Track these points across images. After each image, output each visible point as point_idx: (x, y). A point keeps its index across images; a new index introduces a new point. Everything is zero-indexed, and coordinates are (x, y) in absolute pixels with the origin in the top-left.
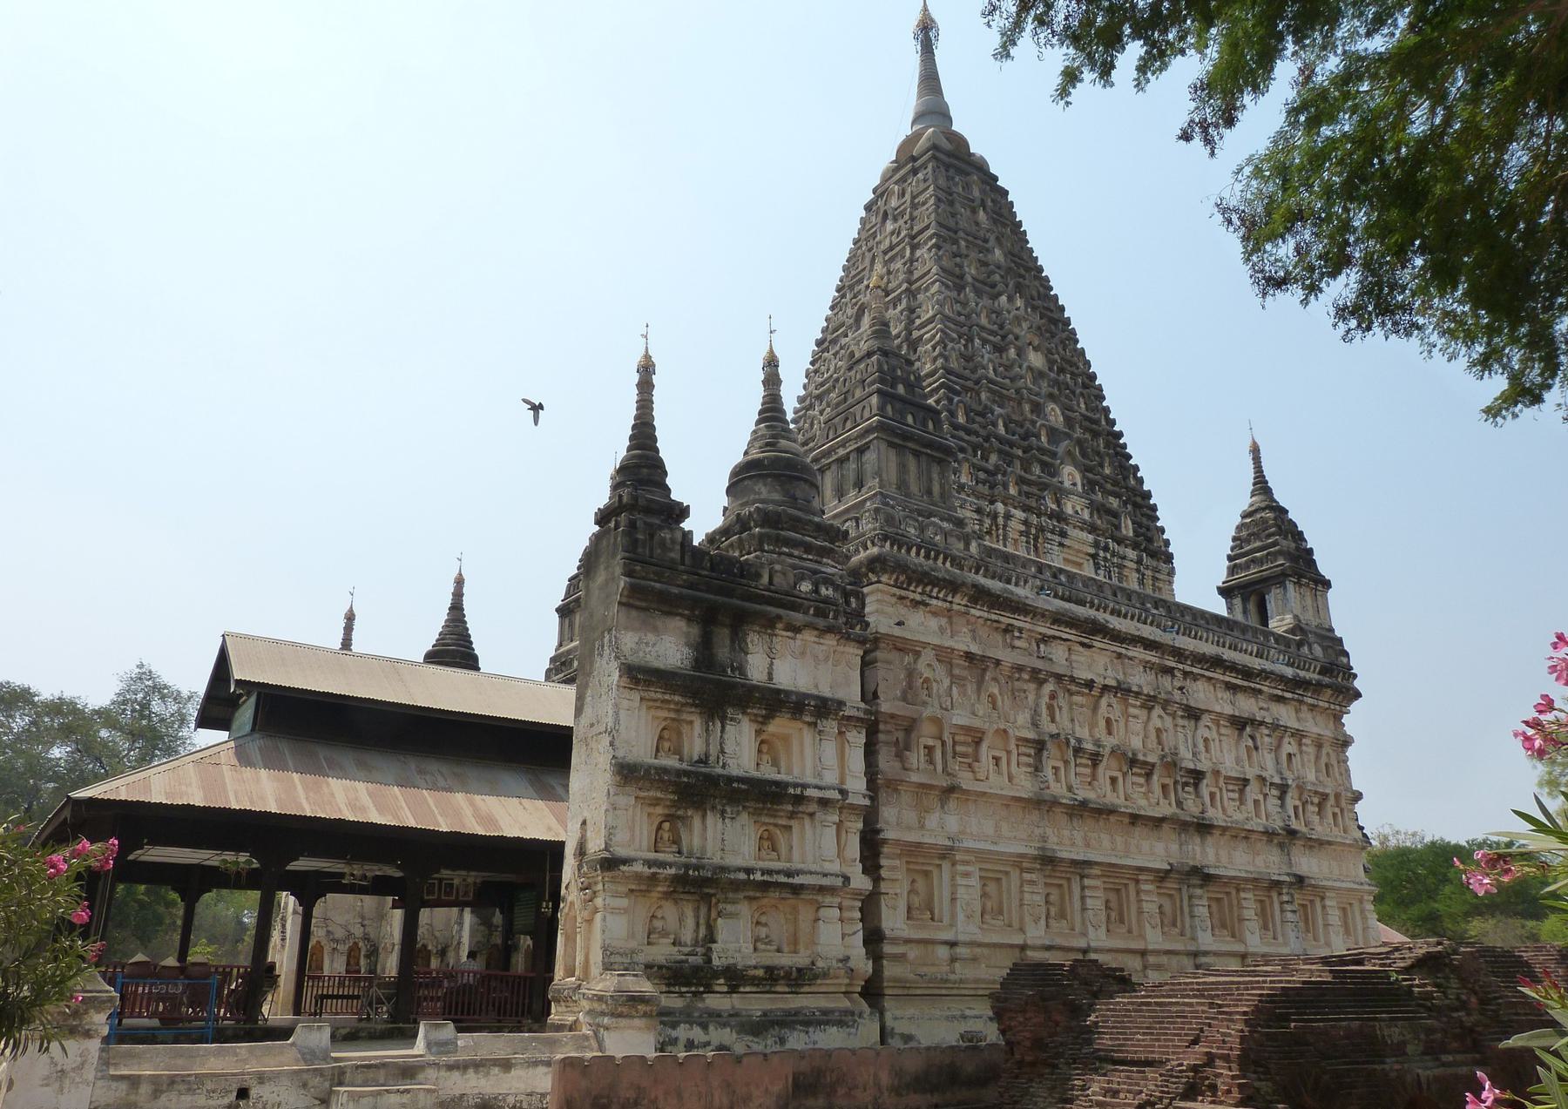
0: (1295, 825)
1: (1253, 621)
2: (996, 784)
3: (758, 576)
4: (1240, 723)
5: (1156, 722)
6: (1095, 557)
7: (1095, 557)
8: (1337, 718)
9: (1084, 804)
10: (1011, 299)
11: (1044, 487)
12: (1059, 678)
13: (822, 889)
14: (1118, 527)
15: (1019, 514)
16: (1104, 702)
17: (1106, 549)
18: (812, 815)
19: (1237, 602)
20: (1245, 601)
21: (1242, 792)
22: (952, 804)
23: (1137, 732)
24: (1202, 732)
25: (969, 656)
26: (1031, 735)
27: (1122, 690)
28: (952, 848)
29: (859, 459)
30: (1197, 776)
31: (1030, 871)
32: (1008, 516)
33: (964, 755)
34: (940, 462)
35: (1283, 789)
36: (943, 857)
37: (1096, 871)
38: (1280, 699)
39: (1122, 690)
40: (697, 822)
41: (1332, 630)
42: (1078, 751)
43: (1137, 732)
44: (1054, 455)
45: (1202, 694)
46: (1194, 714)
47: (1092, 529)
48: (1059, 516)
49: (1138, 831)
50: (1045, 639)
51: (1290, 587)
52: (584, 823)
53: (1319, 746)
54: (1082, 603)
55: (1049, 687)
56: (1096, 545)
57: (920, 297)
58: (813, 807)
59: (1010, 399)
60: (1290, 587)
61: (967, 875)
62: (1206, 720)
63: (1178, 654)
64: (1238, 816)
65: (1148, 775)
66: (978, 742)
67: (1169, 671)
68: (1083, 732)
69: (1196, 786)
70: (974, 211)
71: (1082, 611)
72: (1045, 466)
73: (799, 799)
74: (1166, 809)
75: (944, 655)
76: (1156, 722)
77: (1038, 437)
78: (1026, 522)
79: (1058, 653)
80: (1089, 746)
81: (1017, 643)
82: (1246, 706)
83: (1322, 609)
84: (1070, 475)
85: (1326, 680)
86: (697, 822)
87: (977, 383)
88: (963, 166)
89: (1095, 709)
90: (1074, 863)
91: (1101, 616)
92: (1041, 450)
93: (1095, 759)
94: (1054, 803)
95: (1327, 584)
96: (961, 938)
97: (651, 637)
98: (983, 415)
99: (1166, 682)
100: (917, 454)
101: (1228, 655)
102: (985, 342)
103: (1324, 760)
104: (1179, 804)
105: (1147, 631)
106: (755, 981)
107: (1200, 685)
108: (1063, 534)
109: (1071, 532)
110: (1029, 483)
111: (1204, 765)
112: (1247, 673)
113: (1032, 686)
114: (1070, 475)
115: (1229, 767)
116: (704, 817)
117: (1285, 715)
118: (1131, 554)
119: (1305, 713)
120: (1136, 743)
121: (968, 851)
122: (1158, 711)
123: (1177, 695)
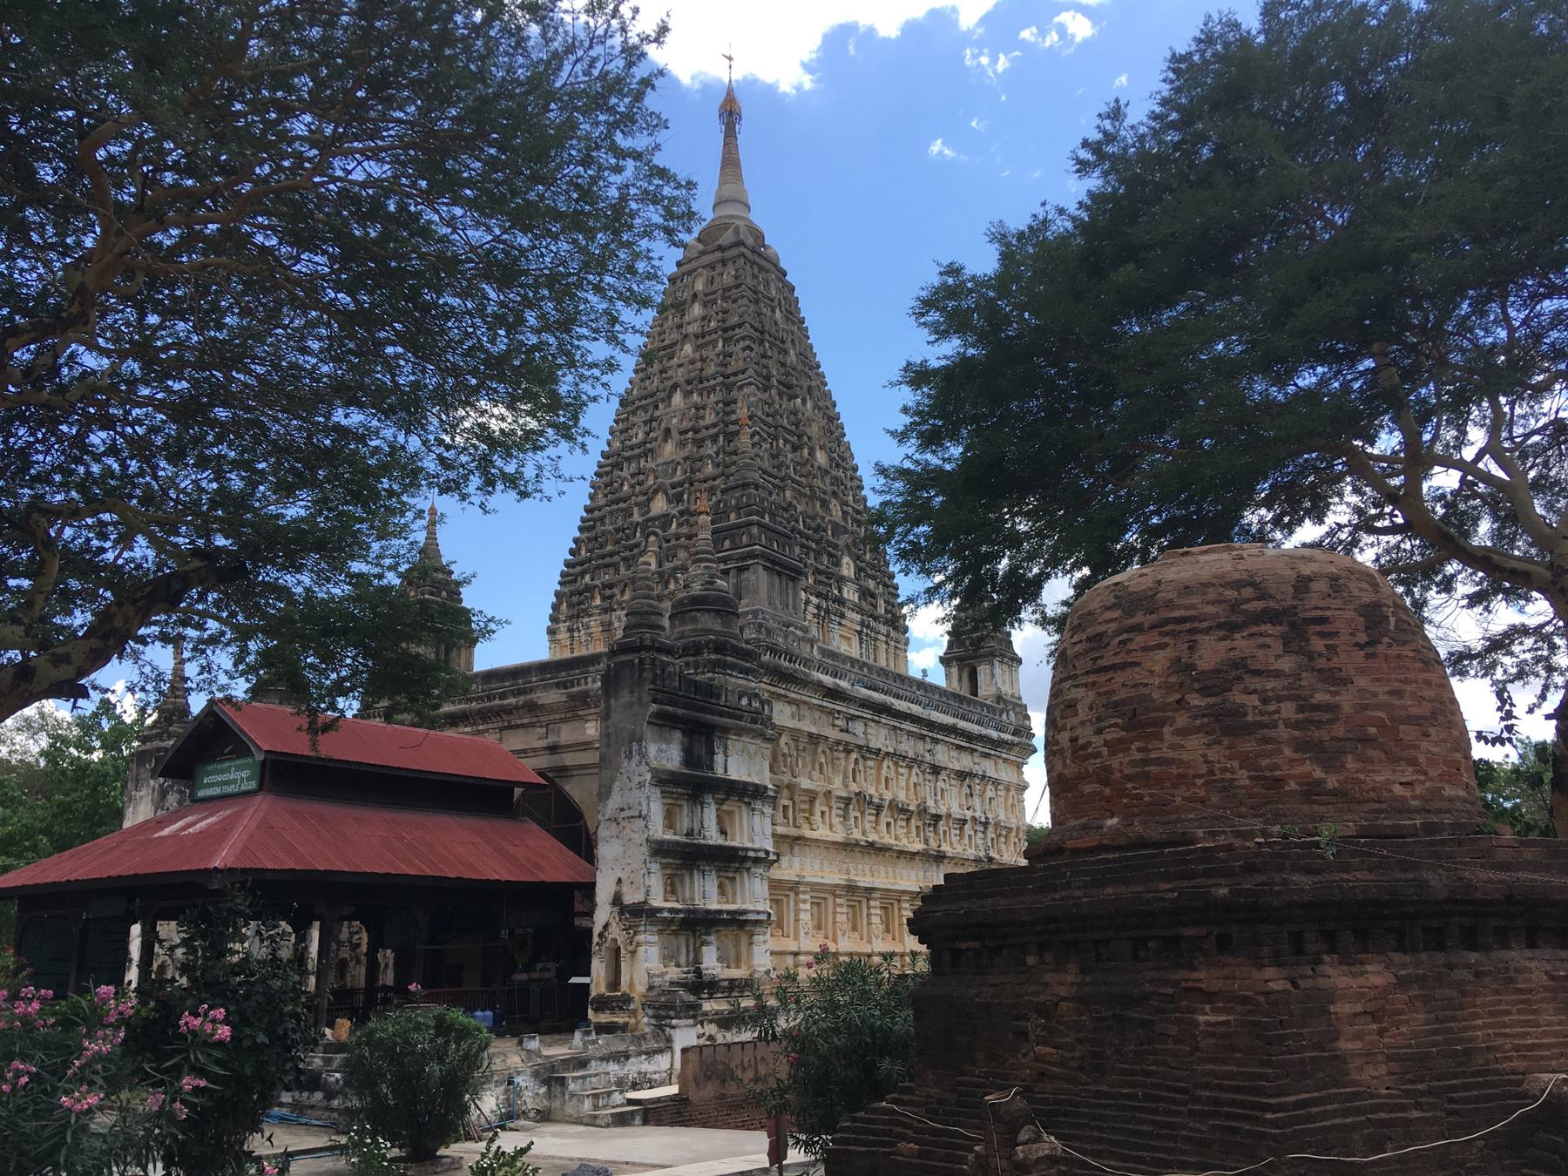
0: (992, 854)
1: (965, 692)
2: (822, 833)
3: (718, 697)
4: (962, 776)
5: (914, 779)
6: (860, 633)
7: (860, 633)
8: (1019, 766)
9: (871, 845)
10: (804, 401)
11: (829, 576)
12: (860, 747)
13: (757, 922)
14: (875, 606)
15: (814, 600)
16: (885, 764)
17: (868, 627)
18: (748, 870)
19: (955, 670)
20: (960, 670)
21: (961, 829)
22: (797, 848)
23: (901, 787)
24: (940, 784)
25: (810, 735)
26: (844, 794)
27: (897, 757)
28: (798, 883)
29: (739, 576)
30: (937, 818)
31: (840, 896)
32: (807, 602)
33: (804, 811)
34: (793, 579)
35: (986, 824)
36: (791, 889)
37: (877, 895)
38: (987, 756)
39: (897, 757)
40: (687, 878)
41: (1020, 698)
42: (870, 803)
43: (901, 787)
44: (836, 547)
45: (943, 755)
46: (936, 770)
47: (860, 611)
48: (841, 601)
49: (902, 863)
50: (853, 718)
51: (997, 664)
52: (620, 881)
53: (1008, 789)
54: (876, 689)
55: (854, 756)
56: (862, 624)
57: (734, 393)
58: (749, 865)
59: (805, 495)
60: (997, 664)
61: (804, 902)
62: (943, 775)
63: (931, 725)
64: (959, 849)
65: (908, 820)
66: (812, 802)
67: (922, 737)
68: (872, 791)
69: (935, 826)
70: (773, 311)
71: (876, 696)
72: (830, 555)
73: (745, 859)
74: (918, 846)
75: (795, 734)
76: (914, 779)
77: (825, 530)
78: (818, 607)
79: (858, 727)
80: (876, 800)
81: (837, 722)
82: (965, 762)
83: (1014, 682)
84: (847, 568)
85: (1016, 739)
86: (687, 878)
87: (782, 480)
88: (762, 262)
89: (880, 768)
90: (867, 889)
91: (890, 700)
92: (830, 544)
93: (879, 808)
94: (857, 844)
95: (1019, 661)
96: (803, 949)
97: (664, 746)
98: (786, 510)
99: (920, 746)
100: (779, 574)
101: (962, 724)
102: (786, 441)
103: (1010, 801)
104: (926, 842)
105: (916, 709)
106: (724, 989)
107: (940, 748)
108: (842, 616)
109: (849, 614)
110: (820, 572)
111: (943, 810)
112: (970, 737)
113: (842, 755)
114: (847, 568)
115: (957, 812)
116: (691, 875)
117: (988, 767)
118: (883, 629)
119: (1001, 765)
120: (902, 796)
121: (807, 884)
122: (915, 770)
123: (928, 758)
